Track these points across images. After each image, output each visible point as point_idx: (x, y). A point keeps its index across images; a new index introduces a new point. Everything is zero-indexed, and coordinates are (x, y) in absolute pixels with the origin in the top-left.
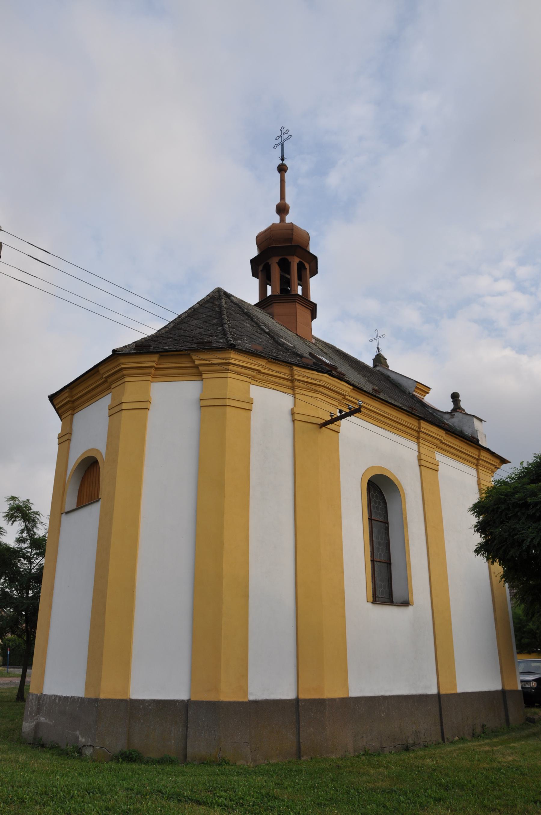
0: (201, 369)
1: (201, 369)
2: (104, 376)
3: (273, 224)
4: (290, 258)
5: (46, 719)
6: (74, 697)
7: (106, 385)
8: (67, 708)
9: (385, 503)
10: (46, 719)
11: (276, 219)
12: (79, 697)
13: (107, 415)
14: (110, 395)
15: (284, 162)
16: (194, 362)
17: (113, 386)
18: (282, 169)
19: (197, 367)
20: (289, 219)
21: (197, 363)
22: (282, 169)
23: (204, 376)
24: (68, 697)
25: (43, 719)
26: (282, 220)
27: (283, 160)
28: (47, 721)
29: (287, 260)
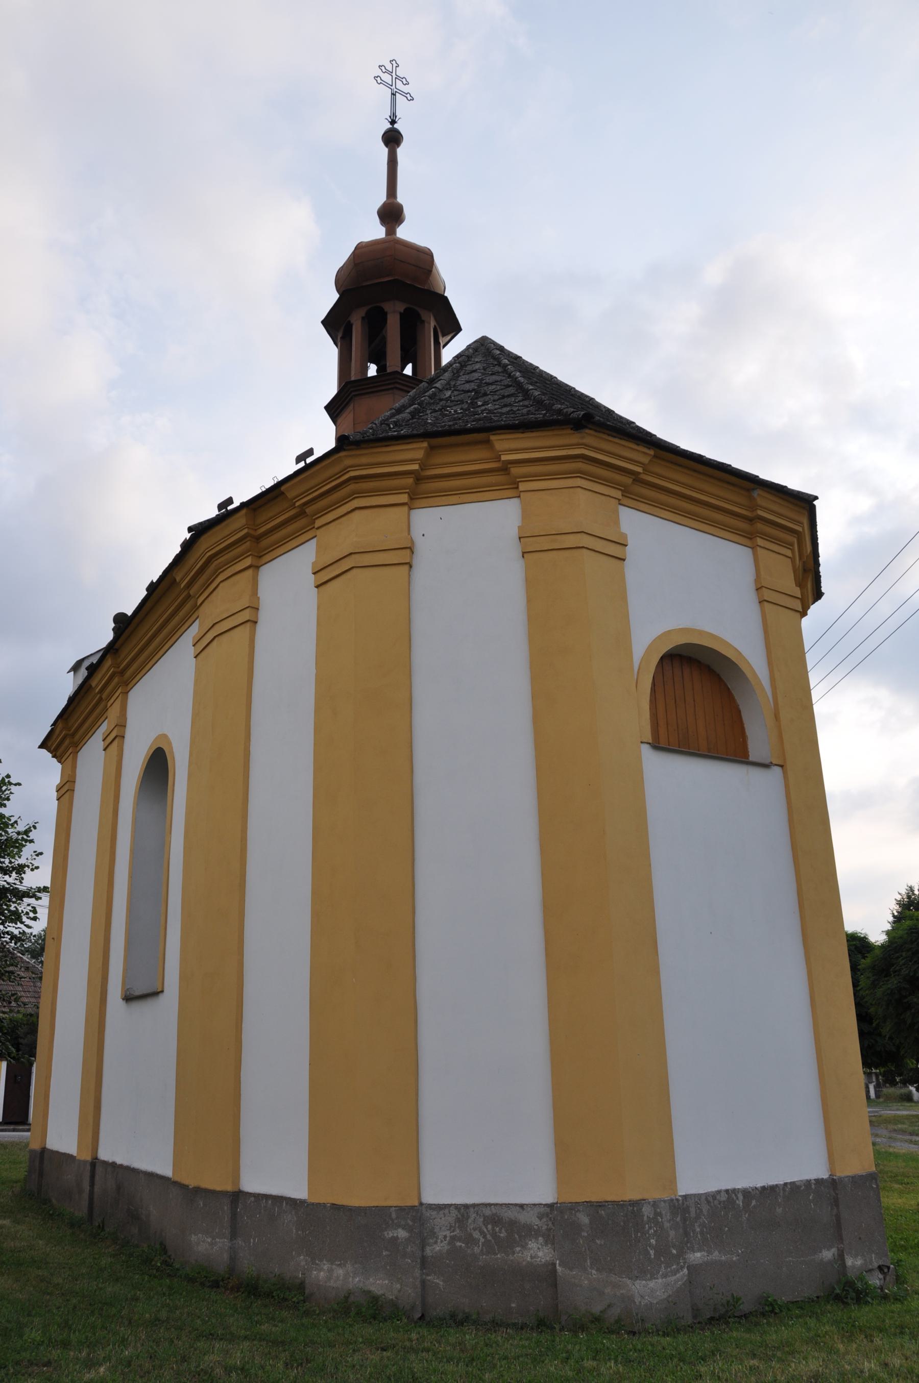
0: (515, 471)
1: (515, 471)
2: (297, 504)
3: (360, 248)
4: (387, 307)
5: (710, 1253)
6: (793, 1183)
7: (303, 522)
8: (779, 1210)
9: (739, 712)
10: (710, 1253)
11: (378, 232)
12: (809, 1181)
13: (313, 585)
14: (314, 541)
15: (396, 126)
16: (498, 458)
17: (318, 523)
18: (392, 139)
19: (505, 468)
20: (403, 232)
21: (504, 458)
22: (392, 139)
23: (522, 486)
24: (773, 1189)
25: (698, 1255)
26: (391, 231)
27: (393, 122)
28: (716, 1255)
29: (381, 309)
